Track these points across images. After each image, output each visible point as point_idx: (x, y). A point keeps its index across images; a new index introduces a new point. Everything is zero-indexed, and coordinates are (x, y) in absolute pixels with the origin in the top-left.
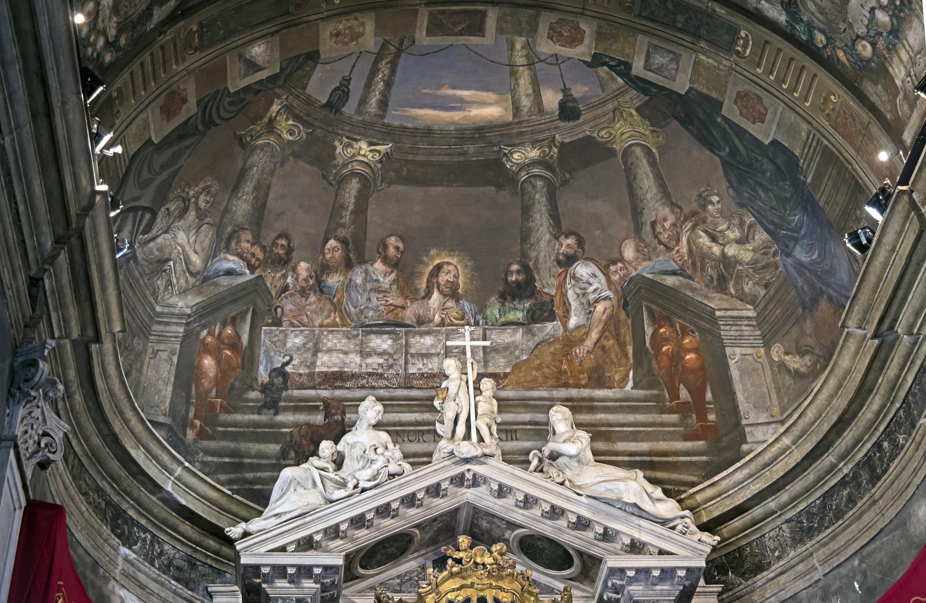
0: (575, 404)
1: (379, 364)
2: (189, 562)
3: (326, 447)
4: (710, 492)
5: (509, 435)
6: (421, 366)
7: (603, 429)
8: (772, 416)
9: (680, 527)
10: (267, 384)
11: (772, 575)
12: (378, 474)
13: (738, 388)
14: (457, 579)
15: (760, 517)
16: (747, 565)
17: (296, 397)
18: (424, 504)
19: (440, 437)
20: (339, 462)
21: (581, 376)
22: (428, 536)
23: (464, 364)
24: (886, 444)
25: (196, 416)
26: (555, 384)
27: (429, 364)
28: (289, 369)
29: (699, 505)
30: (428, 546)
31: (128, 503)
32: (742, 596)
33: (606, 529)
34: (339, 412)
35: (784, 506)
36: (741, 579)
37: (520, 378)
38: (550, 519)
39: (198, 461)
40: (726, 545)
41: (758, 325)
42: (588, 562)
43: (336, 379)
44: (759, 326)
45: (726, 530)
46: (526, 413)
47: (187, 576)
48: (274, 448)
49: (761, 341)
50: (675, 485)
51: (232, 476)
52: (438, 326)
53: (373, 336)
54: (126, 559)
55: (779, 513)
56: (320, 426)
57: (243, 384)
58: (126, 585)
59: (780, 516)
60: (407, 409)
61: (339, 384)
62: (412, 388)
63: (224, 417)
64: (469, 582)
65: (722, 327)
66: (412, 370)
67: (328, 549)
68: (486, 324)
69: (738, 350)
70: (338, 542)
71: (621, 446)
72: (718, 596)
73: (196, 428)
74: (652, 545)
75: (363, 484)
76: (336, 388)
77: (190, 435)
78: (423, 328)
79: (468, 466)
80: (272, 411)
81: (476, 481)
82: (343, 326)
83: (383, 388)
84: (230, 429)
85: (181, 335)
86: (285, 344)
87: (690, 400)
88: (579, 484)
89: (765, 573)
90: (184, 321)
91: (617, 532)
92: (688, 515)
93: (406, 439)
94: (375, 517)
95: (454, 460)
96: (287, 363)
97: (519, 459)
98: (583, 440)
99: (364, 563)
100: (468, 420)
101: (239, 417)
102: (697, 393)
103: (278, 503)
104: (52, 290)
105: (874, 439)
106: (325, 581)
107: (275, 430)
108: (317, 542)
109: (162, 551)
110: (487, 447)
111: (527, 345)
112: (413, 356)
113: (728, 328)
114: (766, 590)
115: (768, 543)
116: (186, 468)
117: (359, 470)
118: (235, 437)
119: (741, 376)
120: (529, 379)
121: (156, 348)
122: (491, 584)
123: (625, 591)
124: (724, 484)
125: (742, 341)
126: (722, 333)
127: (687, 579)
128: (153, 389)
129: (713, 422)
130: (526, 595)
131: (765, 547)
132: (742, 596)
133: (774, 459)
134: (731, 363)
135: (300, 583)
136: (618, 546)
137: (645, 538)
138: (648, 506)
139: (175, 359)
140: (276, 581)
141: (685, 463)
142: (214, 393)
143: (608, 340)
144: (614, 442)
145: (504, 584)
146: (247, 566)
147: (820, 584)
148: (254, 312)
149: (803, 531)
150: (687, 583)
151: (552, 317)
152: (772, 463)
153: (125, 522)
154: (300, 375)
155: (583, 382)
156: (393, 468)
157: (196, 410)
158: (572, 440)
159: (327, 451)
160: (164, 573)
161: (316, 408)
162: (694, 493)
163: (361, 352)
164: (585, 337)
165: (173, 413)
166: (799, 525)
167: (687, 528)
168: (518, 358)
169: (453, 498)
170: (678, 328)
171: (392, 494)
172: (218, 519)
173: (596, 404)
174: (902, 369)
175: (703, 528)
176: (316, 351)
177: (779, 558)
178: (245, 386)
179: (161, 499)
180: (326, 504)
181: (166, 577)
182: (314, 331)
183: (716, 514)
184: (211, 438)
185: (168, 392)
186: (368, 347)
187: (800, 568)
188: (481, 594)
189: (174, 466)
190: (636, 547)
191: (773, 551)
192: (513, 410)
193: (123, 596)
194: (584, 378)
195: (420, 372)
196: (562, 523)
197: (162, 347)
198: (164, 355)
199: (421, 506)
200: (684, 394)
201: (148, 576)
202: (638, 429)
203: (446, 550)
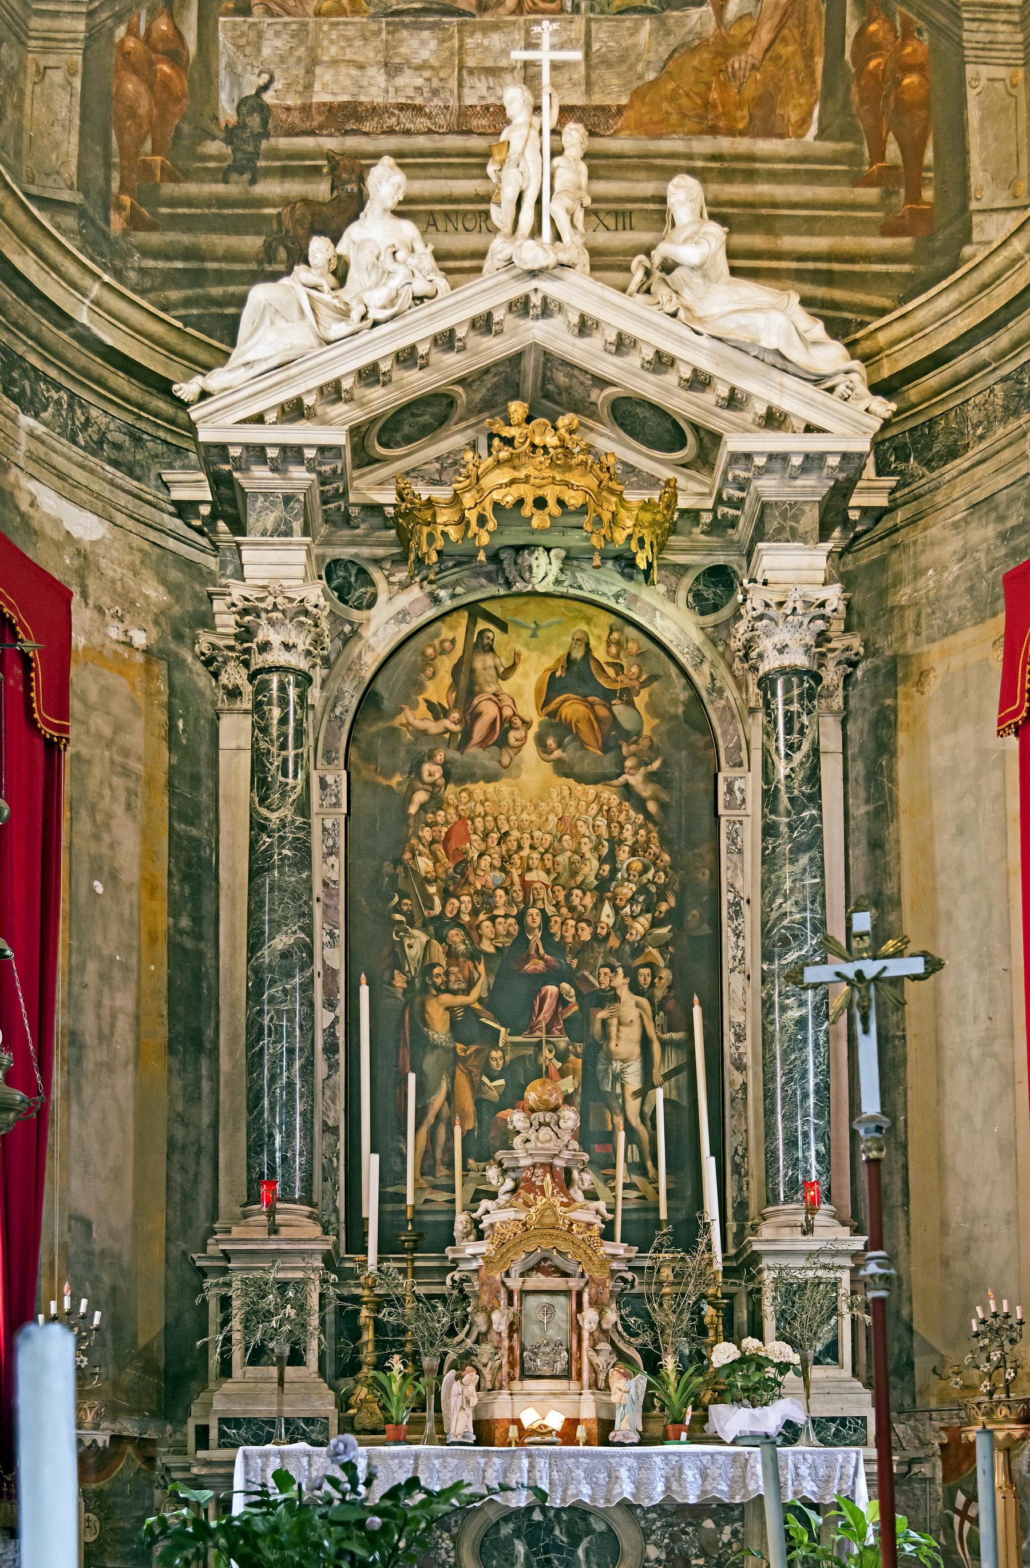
0: (726, 165)
1: (418, 89)
2: (132, 435)
3: (319, 248)
4: (898, 329)
5: (620, 220)
6: (484, 93)
7: (764, 211)
8: (1015, 197)
9: (841, 389)
10: (235, 127)
11: (966, 465)
12: (397, 296)
13: (974, 140)
14: (506, 470)
15: (964, 372)
16: (937, 447)
17: (284, 150)
18: (468, 346)
19: (497, 230)
20: (340, 274)
21: (739, 113)
22: (478, 397)
23: (537, 94)
25: (123, 189)
26: (696, 128)
27: (498, 88)
28: (268, 97)
29: (881, 350)
30: (480, 412)
31: (25, 343)
32: (922, 496)
33: (733, 390)
34: (354, 177)
35: (1001, 355)
36: (924, 469)
37: (641, 115)
38: (654, 371)
39: (132, 268)
40: (912, 415)
42: (707, 440)
43: (348, 118)
45: (913, 392)
46: (648, 180)
47: (131, 458)
48: (253, 243)
49: (1021, 55)
50: (858, 312)
51: (190, 292)
52: (512, 13)
53: (405, 33)
54: (31, 434)
55: (994, 365)
56: (324, 204)
57: (195, 128)
58: (36, 475)
59: (995, 369)
60: (460, 172)
61: (351, 125)
62: (469, 132)
63: (168, 189)
64: (522, 474)
65: (967, 25)
67: (327, 418)
68: (592, 9)
69: (985, 71)
70: (341, 408)
71: (789, 242)
72: (890, 494)
73: (125, 209)
74: (796, 416)
76: (347, 133)
77: (117, 222)
78: (488, 18)
79: (535, 283)
80: (247, 176)
82: (355, 12)
83: (424, 133)
84: (180, 211)
85: (82, 36)
86: (259, 50)
87: (900, 162)
88: (700, 314)
90: (84, 9)
91: (749, 396)
92: (857, 368)
93: (460, 227)
94: (395, 368)
95: (513, 273)
96: (265, 88)
98: (712, 240)
99: (384, 439)
100: (539, 202)
101: (192, 188)
102: (912, 151)
103: (249, 344)
106: (323, 468)
107: (253, 211)
108: (309, 408)
109: (88, 419)
110: (564, 250)
111: (656, 52)
112: (471, 72)
113: (974, 26)
114: (955, 487)
115: (971, 414)
116: (106, 284)
117: (370, 289)
118: (188, 224)
119: (982, 120)
120: (656, 117)
121: (42, 64)
122: (554, 478)
123: (752, 489)
124: (920, 316)
125: (993, 54)
126: (965, 35)
127: (841, 470)
128: (46, 141)
129: (928, 203)
130: (604, 493)
131: (965, 420)
132: (922, 496)
133: (997, 276)
134: (971, 94)
135: (286, 471)
136: (749, 417)
137: (785, 404)
138: (796, 354)
139: (77, 82)
140: (253, 468)
141: (877, 275)
142: (148, 145)
143: (787, 45)
144: (777, 235)
145: (574, 478)
146: (208, 446)
149: (1021, 397)
150: (841, 476)
152: (992, 282)
153: (25, 374)
154: (288, 109)
155: (741, 126)
156: (420, 287)
157: (121, 178)
158: (696, 238)
159: (319, 255)
160: (94, 454)
161: (316, 170)
162: (876, 330)
163: (386, 65)
164: (750, 37)
165: (83, 186)
166: (1018, 386)
167: (852, 390)
168: (640, 77)
169: (512, 337)
170: (898, 24)
172: (166, 366)
173: (758, 165)
175: (875, 389)
177: (982, 438)
178: (199, 131)
179: (76, 337)
180: (321, 345)
181: (96, 461)
182: (306, 24)
183: (903, 364)
184: (151, 227)
185: (72, 146)
186: (397, 54)
187: (1007, 455)
188: (540, 492)
189: (87, 282)
190: (773, 420)
191: (976, 426)
192: (629, 175)
193: (33, 491)
194: (744, 117)
195: (483, 103)
196: (671, 379)
197: (52, 60)
198: (56, 77)
199: (464, 348)
200: (893, 151)
201: (69, 459)
202: (816, 213)
203: (491, 424)
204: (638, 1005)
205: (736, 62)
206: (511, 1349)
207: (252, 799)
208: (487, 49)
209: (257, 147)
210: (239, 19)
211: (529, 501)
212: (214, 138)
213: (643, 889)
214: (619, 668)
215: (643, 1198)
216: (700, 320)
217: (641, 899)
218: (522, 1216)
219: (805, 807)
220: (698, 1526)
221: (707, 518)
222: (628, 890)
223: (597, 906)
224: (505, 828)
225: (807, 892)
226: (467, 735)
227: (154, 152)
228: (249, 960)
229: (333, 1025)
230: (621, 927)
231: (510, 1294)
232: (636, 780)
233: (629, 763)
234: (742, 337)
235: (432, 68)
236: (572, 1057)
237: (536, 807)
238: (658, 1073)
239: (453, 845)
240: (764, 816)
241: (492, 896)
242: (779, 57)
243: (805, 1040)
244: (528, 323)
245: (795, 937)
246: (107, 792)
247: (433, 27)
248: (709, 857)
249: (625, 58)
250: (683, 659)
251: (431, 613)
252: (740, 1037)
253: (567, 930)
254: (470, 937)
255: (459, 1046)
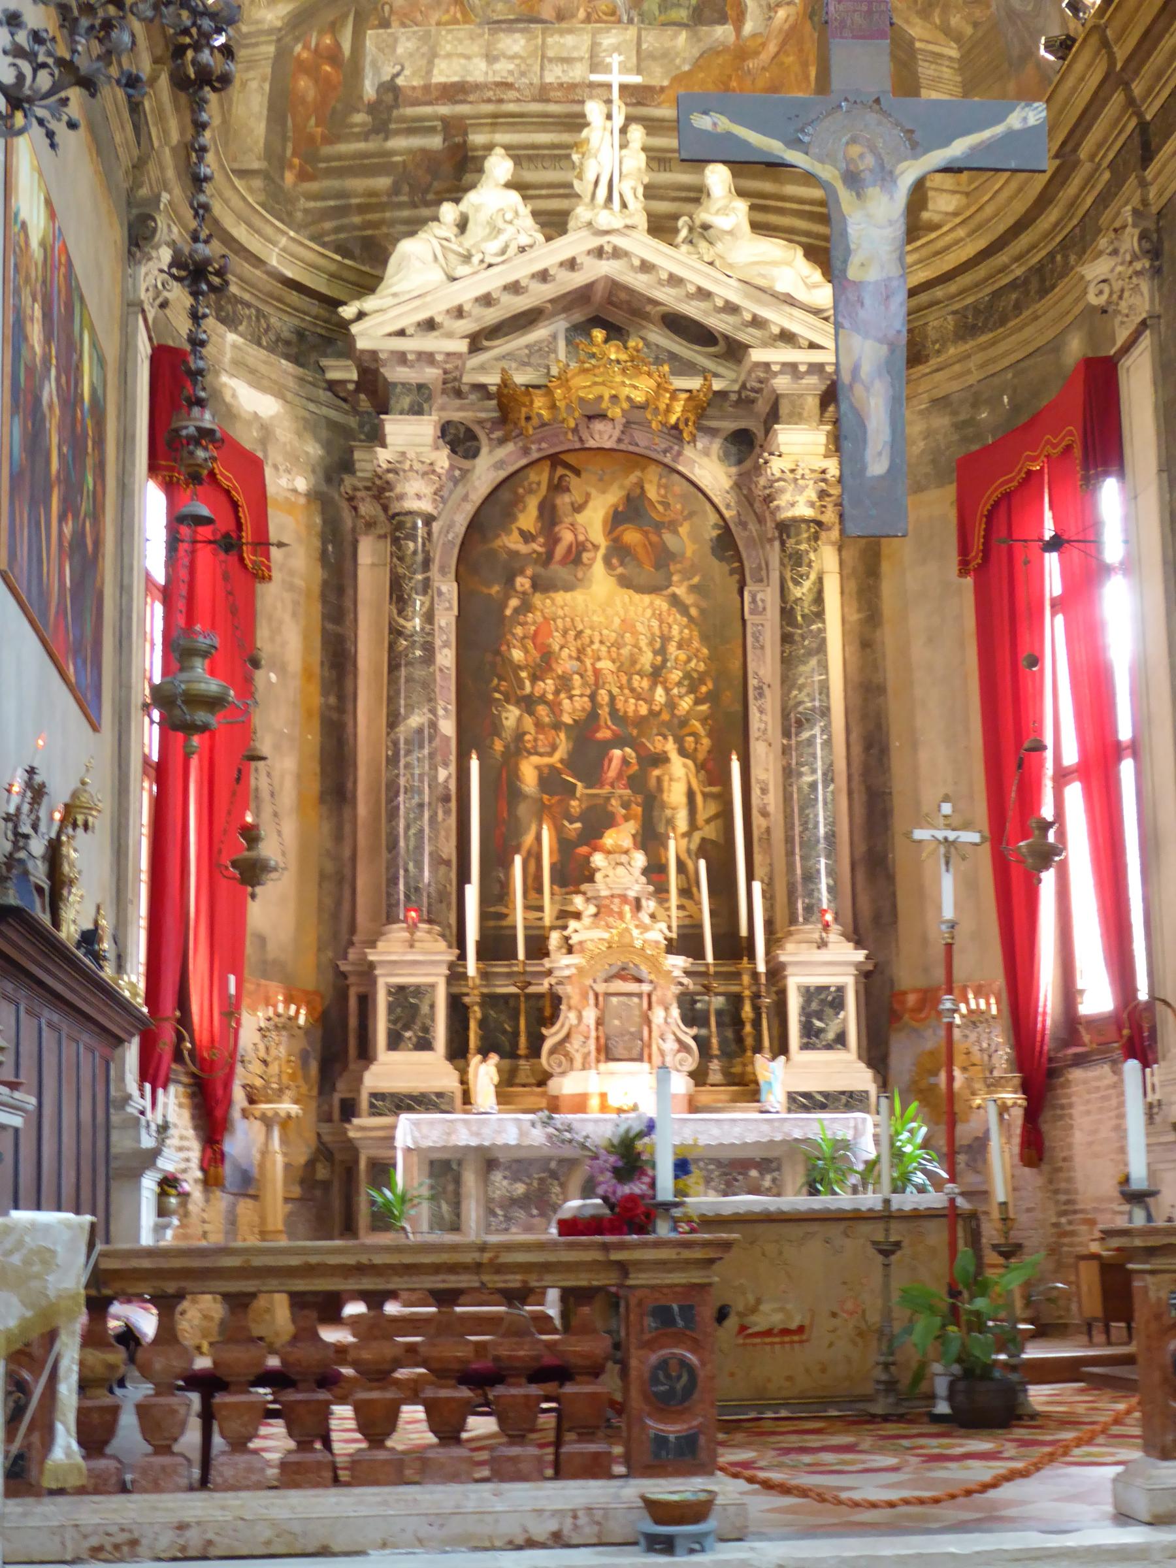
20: (462, 225)
24: (1059, 258)
25: (295, 154)
28: (400, 81)
41: (960, 69)
44: (961, 70)
48: (383, 182)
52: (583, 22)
53: (502, 35)
61: (460, 97)
62: (548, 101)
63: (326, 150)
66: (549, 78)
68: (642, 22)
75: (489, 260)
77: (289, 177)
78: (564, 25)
80: (382, 136)
81: (618, 253)
82: (466, 22)
86: (394, 50)
89: (921, 367)
96: (398, 75)
97: (661, 227)
104: (152, 110)
105: (1050, 248)
112: (550, 60)
113: (926, 64)
118: (341, 173)
131: (926, 337)
133: (946, 249)
137: (795, 328)
142: (313, 121)
147: (973, 390)
148: (357, 15)
151: (722, 20)
154: (414, 88)
156: (524, 240)
168: (678, 68)
171: (521, 270)
174: (1082, 189)
176: (433, 56)
177: (939, 352)
184: (311, 178)
187: (957, 368)
190: (787, 337)
191: (934, 343)
197: (251, 74)
198: (254, 85)
204: (685, 766)
205: (751, 64)
206: (598, 1038)
207: (390, 611)
208: (564, 45)
209: (390, 115)
210: (381, 31)
211: (606, 397)
212: (358, 111)
213: (687, 675)
214: (666, 505)
215: (690, 916)
216: (731, 266)
217: (686, 683)
218: (606, 936)
219: (813, 622)
220: (745, 1174)
221: (734, 397)
222: (676, 675)
223: (652, 688)
224: (580, 627)
225: (816, 686)
226: (550, 555)
227: (317, 125)
228: (388, 734)
229: (446, 781)
230: (671, 705)
231: (596, 995)
232: (680, 591)
233: (675, 578)
234: (761, 282)
235: (521, 57)
236: (634, 806)
237: (604, 611)
238: (701, 816)
239: (539, 640)
240: (782, 627)
241: (570, 680)
242: (782, 63)
243: (816, 799)
244: (603, 262)
245: (808, 720)
246: (279, 605)
247: (522, 31)
248: (740, 651)
249: (665, 56)
250: (716, 500)
251: (523, 462)
252: (764, 791)
253: (632, 707)
254: (553, 712)
255: (546, 797)
